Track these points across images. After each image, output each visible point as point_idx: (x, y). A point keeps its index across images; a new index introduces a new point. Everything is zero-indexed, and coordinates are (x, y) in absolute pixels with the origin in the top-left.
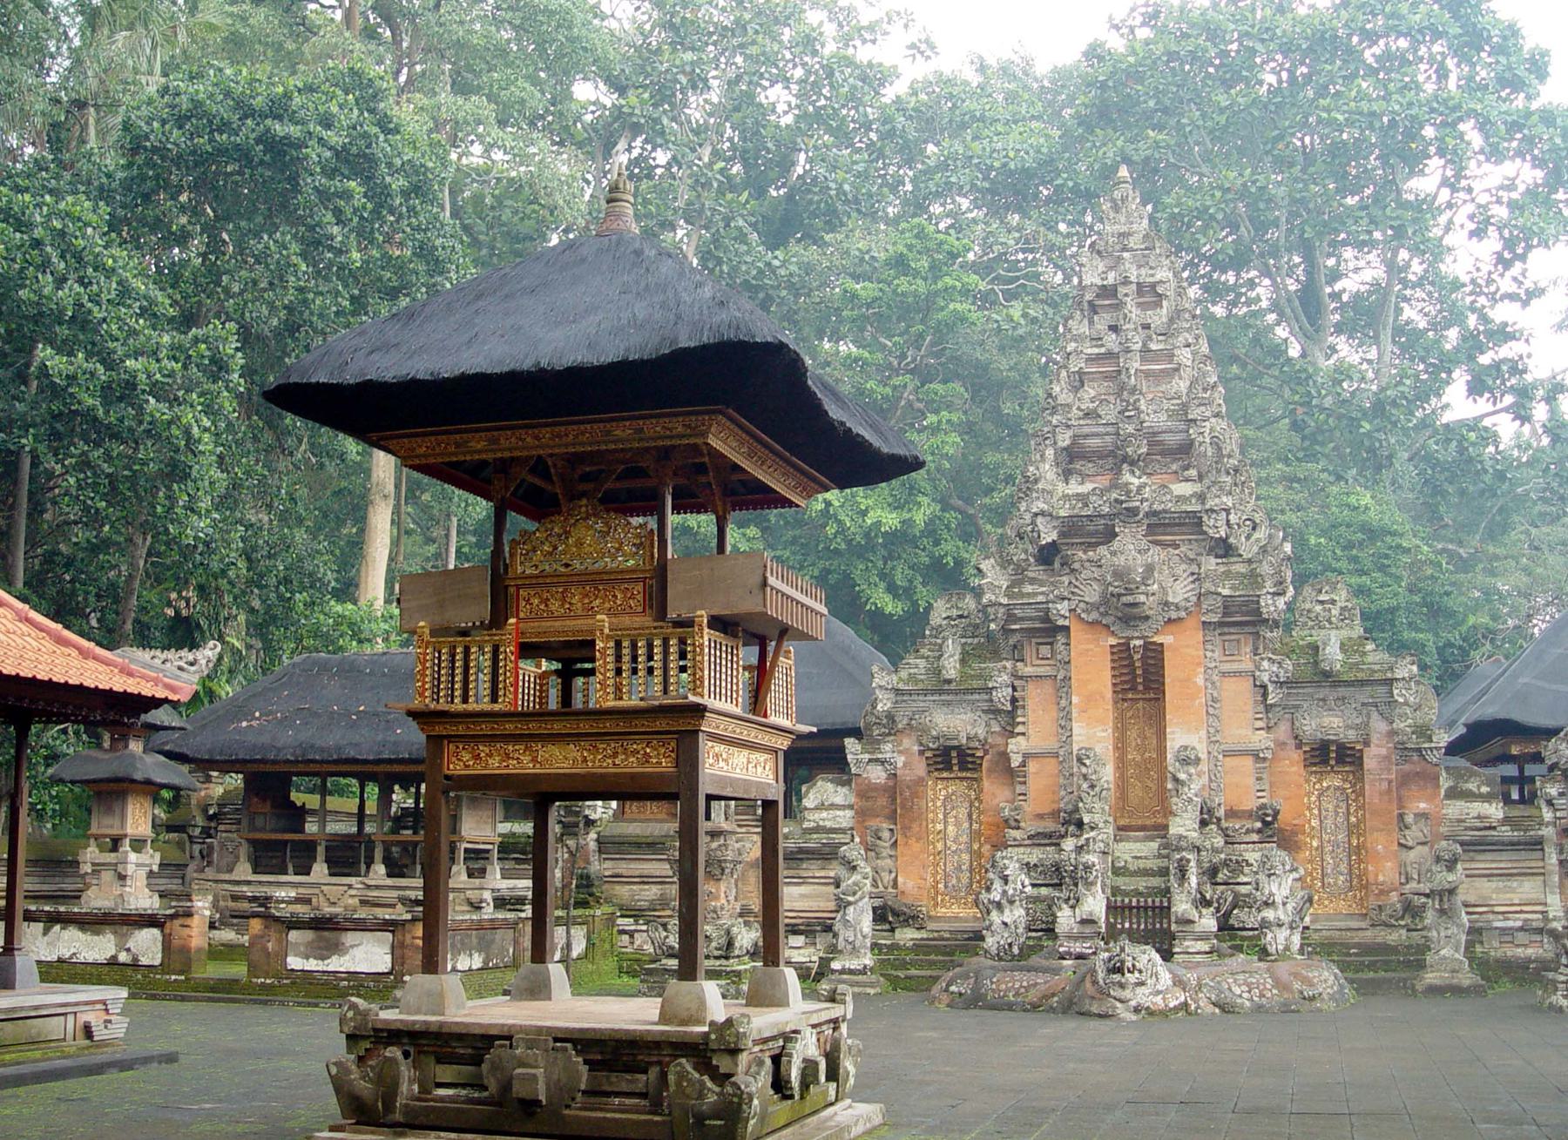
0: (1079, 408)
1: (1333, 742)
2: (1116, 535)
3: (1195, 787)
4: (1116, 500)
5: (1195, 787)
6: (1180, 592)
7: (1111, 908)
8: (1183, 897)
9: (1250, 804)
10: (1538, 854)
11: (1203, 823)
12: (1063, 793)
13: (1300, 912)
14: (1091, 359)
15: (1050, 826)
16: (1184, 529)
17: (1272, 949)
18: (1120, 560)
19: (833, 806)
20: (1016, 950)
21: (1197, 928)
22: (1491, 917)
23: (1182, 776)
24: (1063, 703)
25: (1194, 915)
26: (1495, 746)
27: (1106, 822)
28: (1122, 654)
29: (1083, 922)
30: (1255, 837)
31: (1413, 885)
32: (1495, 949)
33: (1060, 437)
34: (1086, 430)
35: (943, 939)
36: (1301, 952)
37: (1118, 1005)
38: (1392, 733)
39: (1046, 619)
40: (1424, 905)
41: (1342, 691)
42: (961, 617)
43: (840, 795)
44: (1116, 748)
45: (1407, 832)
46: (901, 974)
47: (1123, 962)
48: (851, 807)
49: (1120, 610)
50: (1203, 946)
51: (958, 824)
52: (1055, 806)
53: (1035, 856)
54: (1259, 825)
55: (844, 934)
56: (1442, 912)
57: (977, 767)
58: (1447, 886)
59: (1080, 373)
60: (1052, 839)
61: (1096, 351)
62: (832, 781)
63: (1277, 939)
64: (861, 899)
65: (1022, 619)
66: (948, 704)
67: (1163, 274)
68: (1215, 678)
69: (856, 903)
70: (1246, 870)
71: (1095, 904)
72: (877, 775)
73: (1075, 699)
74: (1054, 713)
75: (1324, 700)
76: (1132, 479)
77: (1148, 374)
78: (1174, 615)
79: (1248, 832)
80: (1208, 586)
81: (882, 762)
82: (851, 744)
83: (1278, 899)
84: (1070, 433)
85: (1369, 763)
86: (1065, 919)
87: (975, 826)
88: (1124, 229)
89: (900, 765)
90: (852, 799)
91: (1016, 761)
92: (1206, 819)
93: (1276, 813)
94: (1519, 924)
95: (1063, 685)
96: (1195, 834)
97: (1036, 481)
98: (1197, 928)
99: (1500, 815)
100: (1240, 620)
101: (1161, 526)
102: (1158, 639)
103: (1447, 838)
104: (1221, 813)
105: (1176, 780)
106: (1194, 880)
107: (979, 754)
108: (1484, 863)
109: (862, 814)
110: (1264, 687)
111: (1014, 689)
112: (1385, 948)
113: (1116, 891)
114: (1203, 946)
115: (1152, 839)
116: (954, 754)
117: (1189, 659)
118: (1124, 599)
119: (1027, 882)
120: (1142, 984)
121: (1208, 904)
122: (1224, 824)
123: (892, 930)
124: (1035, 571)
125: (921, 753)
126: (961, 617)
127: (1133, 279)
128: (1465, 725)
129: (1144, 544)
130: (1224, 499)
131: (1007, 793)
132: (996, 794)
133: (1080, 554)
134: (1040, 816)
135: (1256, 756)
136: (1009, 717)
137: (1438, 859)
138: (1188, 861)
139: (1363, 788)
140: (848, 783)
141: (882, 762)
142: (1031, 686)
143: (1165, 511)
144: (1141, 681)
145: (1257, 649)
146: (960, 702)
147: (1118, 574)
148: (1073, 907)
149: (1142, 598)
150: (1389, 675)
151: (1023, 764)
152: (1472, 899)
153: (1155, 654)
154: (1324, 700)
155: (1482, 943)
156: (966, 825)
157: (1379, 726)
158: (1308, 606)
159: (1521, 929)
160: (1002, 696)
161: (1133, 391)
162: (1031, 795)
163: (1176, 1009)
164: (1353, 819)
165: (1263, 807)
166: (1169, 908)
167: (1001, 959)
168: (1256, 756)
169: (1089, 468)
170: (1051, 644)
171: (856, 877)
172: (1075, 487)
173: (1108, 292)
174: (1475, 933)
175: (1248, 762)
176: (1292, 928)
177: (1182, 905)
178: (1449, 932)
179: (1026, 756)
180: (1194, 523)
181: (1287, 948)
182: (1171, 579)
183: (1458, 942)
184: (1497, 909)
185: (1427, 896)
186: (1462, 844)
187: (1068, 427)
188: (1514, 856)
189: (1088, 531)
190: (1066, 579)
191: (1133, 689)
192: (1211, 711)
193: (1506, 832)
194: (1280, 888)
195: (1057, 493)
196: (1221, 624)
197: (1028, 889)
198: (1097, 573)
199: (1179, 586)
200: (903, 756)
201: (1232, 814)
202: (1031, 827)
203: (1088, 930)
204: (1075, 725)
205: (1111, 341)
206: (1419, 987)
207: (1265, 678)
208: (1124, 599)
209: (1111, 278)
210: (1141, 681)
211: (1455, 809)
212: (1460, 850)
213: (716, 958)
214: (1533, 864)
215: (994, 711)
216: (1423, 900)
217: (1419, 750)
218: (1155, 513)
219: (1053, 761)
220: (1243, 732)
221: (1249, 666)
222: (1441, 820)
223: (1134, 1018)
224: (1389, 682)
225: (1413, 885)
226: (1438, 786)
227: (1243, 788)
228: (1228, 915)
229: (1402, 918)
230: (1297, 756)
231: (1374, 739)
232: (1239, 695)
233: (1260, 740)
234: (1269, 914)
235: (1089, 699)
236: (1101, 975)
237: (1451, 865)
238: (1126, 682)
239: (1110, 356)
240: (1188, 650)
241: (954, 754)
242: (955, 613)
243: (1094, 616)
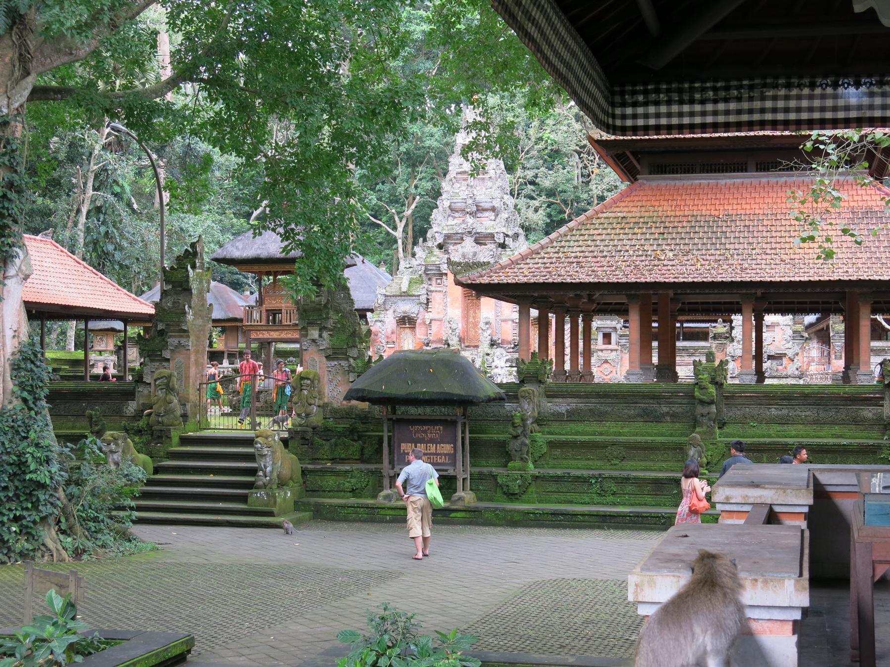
82: (369, 314)
142: (434, 294)
160: (423, 299)
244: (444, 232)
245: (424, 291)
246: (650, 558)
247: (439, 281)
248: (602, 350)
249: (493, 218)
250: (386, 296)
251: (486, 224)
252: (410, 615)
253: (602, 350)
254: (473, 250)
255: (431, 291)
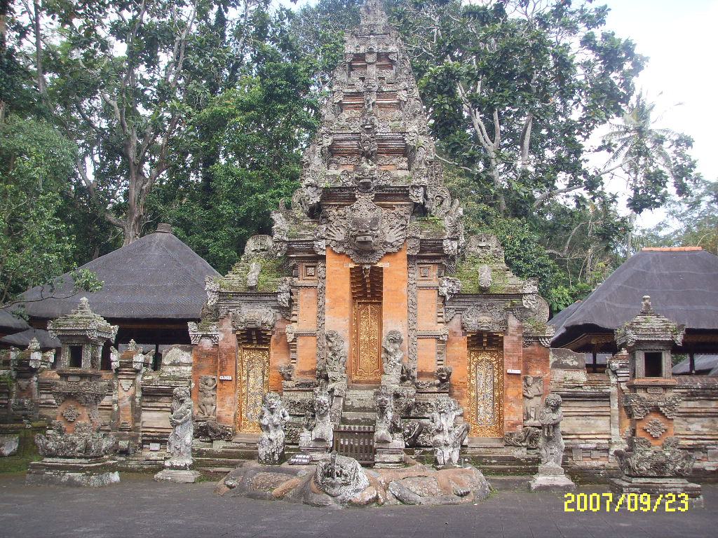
0: (337, 124)
1: (485, 331)
2: (356, 199)
3: (399, 356)
4: (356, 178)
5: (399, 356)
6: (392, 236)
7: (337, 432)
8: (383, 425)
9: (433, 367)
10: (607, 404)
11: (403, 380)
12: (318, 359)
13: (461, 437)
14: (348, 96)
15: (310, 379)
16: (398, 198)
17: (440, 460)
18: (357, 215)
19: (179, 364)
20: (276, 457)
21: (391, 446)
22: (577, 441)
23: (391, 350)
24: (321, 303)
25: (389, 437)
26: (581, 340)
27: (342, 377)
28: (356, 274)
29: (317, 440)
30: (436, 389)
31: (531, 422)
32: (581, 462)
33: (325, 140)
34: (341, 137)
35: (242, 448)
36: (459, 462)
37: (330, 498)
38: (521, 328)
39: (312, 251)
40: (537, 434)
41: (491, 301)
42: (263, 250)
43: (186, 357)
44: (351, 333)
45: (528, 388)
46: (211, 470)
47: (333, 469)
48: (190, 364)
49: (361, 248)
50: (395, 458)
51: (256, 377)
52: (313, 367)
53: (299, 397)
54: (438, 381)
55: (175, 443)
56: (549, 439)
57: (267, 342)
58: (553, 422)
59: (340, 103)
60: (306, 387)
61: (351, 91)
62: (181, 348)
63: (444, 454)
64: (186, 421)
65: (297, 251)
66: (250, 302)
67: (392, 48)
68: (414, 290)
69: (181, 424)
70: (429, 410)
71: (326, 428)
72: (207, 344)
73: (327, 301)
74: (315, 309)
75: (481, 306)
76: (367, 166)
77: (381, 106)
78: (389, 250)
79: (431, 385)
80: (411, 233)
81: (210, 337)
82: (192, 326)
83: (446, 428)
84: (331, 138)
85: (507, 345)
86: (306, 438)
87: (266, 378)
88: (372, 23)
89: (220, 339)
90: (191, 360)
91: (290, 338)
92: (405, 377)
93: (449, 374)
94: (594, 446)
95: (321, 292)
96: (397, 386)
97: (308, 165)
98: (391, 446)
99: (585, 379)
100: (430, 253)
101: (385, 195)
102: (379, 265)
103: (553, 392)
104: (415, 373)
105: (387, 352)
106: (390, 415)
107: (269, 334)
108: (576, 407)
109: (196, 369)
110: (444, 297)
111: (291, 294)
112: (513, 460)
113: (344, 421)
114: (395, 458)
115: (371, 388)
116: (254, 333)
117: (395, 273)
118: (359, 238)
119: (286, 413)
120: (347, 484)
121: (399, 430)
122: (417, 381)
123: (211, 441)
124: (307, 222)
125: (234, 332)
126: (263, 250)
127: (375, 50)
128: (567, 328)
129: (373, 205)
130: (423, 180)
131: (286, 360)
132: (279, 360)
133: (334, 211)
134: (303, 373)
135: (437, 338)
136: (287, 311)
137: (547, 405)
138: (386, 402)
139: (502, 362)
140: (189, 350)
141: (210, 337)
142: (301, 292)
143: (386, 186)
144: (368, 289)
145: (440, 273)
146: (259, 301)
147: (356, 223)
148: (311, 430)
149: (369, 238)
150: (520, 291)
151: (295, 340)
152: (566, 430)
153: (377, 274)
154: (481, 306)
155: (572, 457)
156: (261, 378)
157: (513, 322)
158: (473, 249)
159: (596, 449)
160: (283, 298)
161: (370, 114)
162: (299, 359)
163: (369, 503)
164: (496, 380)
165: (441, 370)
166: (374, 432)
167: (267, 463)
168: (437, 338)
169: (343, 160)
170: (315, 267)
171: (183, 407)
172: (333, 171)
173: (359, 57)
174: (568, 450)
175: (433, 342)
176: (454, 447)
177: (382, 431)
178: (553, 451)
179: (297, 335)
180: (403, 193)
181: (450, 460)
182: (391, 228)
183: (558, 457)
184: (581, 437)
185: (540, 428)
186: (562, 396)
187: (330, 134)
188: (592, 404)
189: (335, 195)
190: (324, 227)
191: (365, 296)
192: (411, 310)
193: (588, 390)
194: (446, 422)
195: (319, 173)
196: (418, 257)
197: (288, 418)
198: (344, 222)
199: (392, 233)
200: (225, 334)
201: (421, 374)
202: (297, 378)
203: (320, 445)
204: (326, 316)
205: (360, 86)
206: (534, 486)
207: (445, 291)
208: (359, 238)
209: (362, 50)
210: (368, 289)
211: (560, 374)
212: (561, 400)
213: (79, 458)
214: (603, 410)
215: (281, 308)
216: (538, 430)
217: (537, 338)
218: (380, 187)
219: (313, 338)
220: (430, 324)
221: (436, 284)
222: (547, 382)
223: (340, 508)
224: (520, 296)
225: (531, 422)
226: (548, 361)
227: (427, 359)
228: (416, 437)
229: (524, 441)
230: (464, 340)
231: (511, 330)
232: (428, 302)
233: (441, 329)
234: (439, 438)
235: (336, 301)
236: (319, 478)
237: (555, 408)
238: (360, 292)
239: (358, 94)
240: (398, 273)
241: (254, 333)
242: (259, 248)
243: (341, 249)
244: (323, 185)
245: (284, 287)
246: (354, 304)
247: (311, 270)
248: (645, 388)
249: (405, 165)
250: (220, 294)
251: (396, 172)
252: (580, 8)
253: (645, 388)
254: (370, 215)
255: (298, 287)
